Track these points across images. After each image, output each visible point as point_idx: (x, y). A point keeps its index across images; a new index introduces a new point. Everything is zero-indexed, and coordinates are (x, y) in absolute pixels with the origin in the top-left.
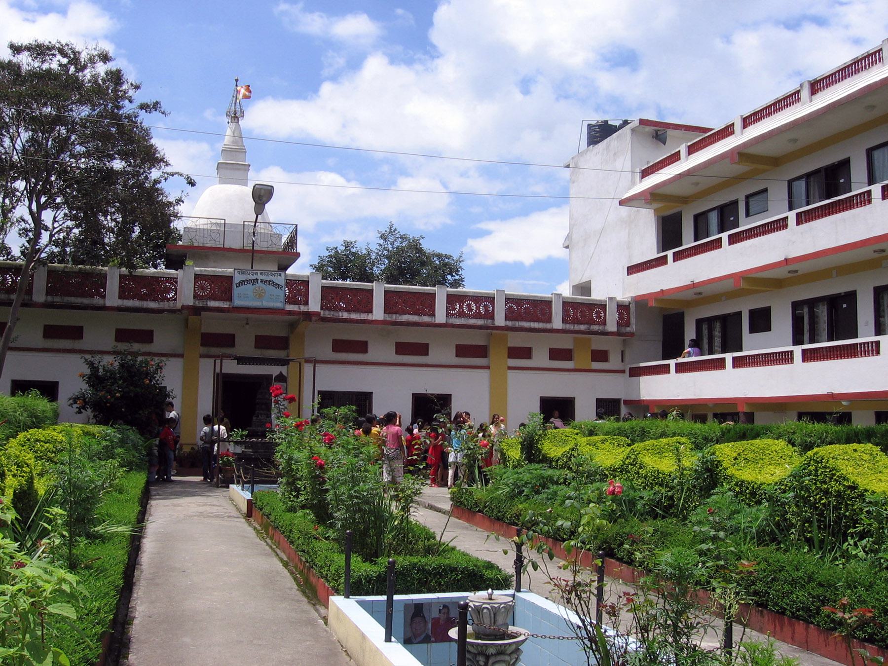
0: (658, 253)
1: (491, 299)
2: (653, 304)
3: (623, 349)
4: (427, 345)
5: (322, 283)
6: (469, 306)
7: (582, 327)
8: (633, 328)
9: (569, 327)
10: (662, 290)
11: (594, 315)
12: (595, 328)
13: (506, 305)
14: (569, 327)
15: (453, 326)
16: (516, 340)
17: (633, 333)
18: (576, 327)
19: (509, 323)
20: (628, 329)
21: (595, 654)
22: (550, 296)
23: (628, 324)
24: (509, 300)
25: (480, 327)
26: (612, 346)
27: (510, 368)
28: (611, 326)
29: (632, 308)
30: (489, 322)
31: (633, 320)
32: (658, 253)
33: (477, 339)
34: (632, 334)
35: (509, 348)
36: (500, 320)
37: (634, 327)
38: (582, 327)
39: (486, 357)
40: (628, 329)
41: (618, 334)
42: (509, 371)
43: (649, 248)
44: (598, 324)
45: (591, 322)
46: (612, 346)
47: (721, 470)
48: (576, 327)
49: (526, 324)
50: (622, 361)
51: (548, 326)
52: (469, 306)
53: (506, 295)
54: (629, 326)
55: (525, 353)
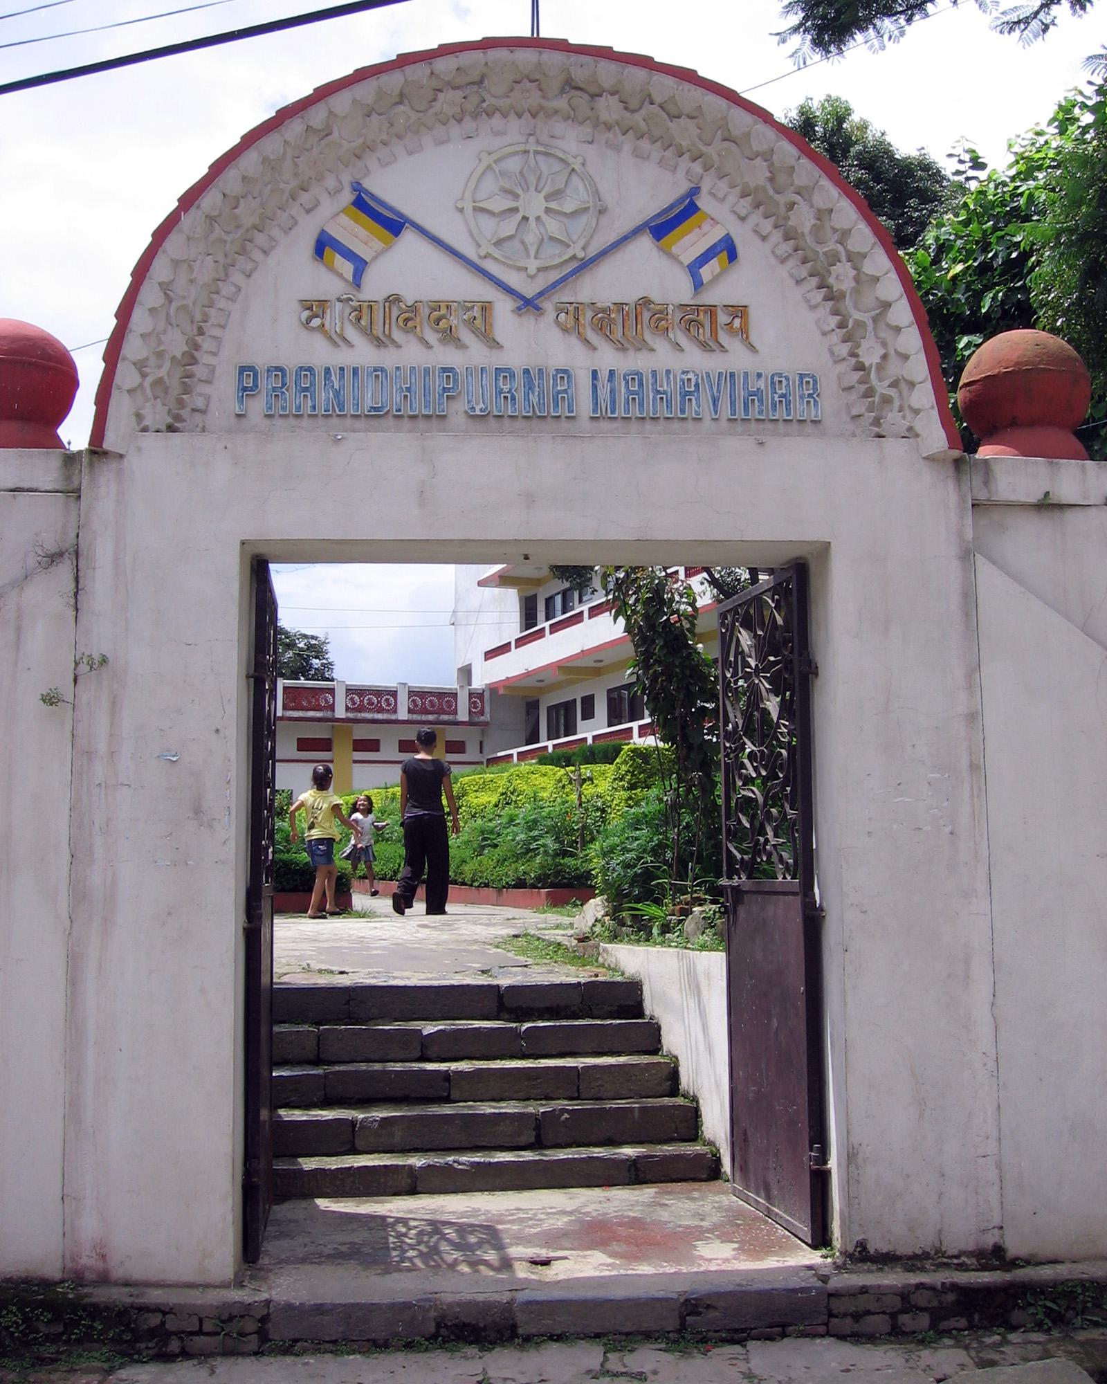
0: (521, 632)
1: (394, 694)
2: (501, 692)
3: (481, 739)
4: (378, 741)
5: (284, 683)
6: (387, 700)
7: (431, 717)
8: (486, 717)
9: (416, 717)
10: (507, 678)
11: (365, 702)
12: (445, 717)
13: (409, 698)
14: (416, 717)
15: (290, 719)
16: (361, 733)
17: (488, 723)
18: (425, 718)
19: (351, 715)
20: (482, 718)
21: (689, 948)
22: (395, 685)
23: (482, 713)
24: (413, 693)
25: (319, 720)
26: (470, 737)
27: (355, 762)
28: (463, 716)
29: (487, 696)
30: (328, 714)
31: (487, 709)
32: (521, 632)
33: (320, 732)
34: (486, 724)
35: (355, 741)
36: (340, 712)
37: (489, 716)
38: (431, 717)
39: (330, 751)
40: (482, 718)
41: (470, 723)
42: (354, 765)
43: (512, 628)
44: (388, 711)
45: (441, 711)
46: (470, 737)
47: (591, 848)
48: (425, 718)
49: (369, 716)
50: (481, 752)
51: (393, 717)
52: (387, 700)
53: (347, 685)
54: (482, 715)
55: (373, 746)
